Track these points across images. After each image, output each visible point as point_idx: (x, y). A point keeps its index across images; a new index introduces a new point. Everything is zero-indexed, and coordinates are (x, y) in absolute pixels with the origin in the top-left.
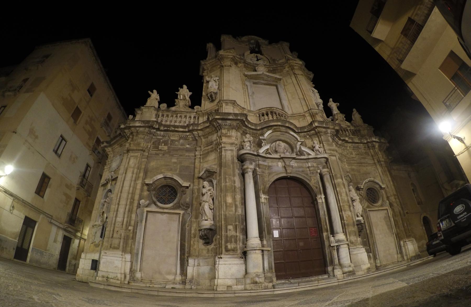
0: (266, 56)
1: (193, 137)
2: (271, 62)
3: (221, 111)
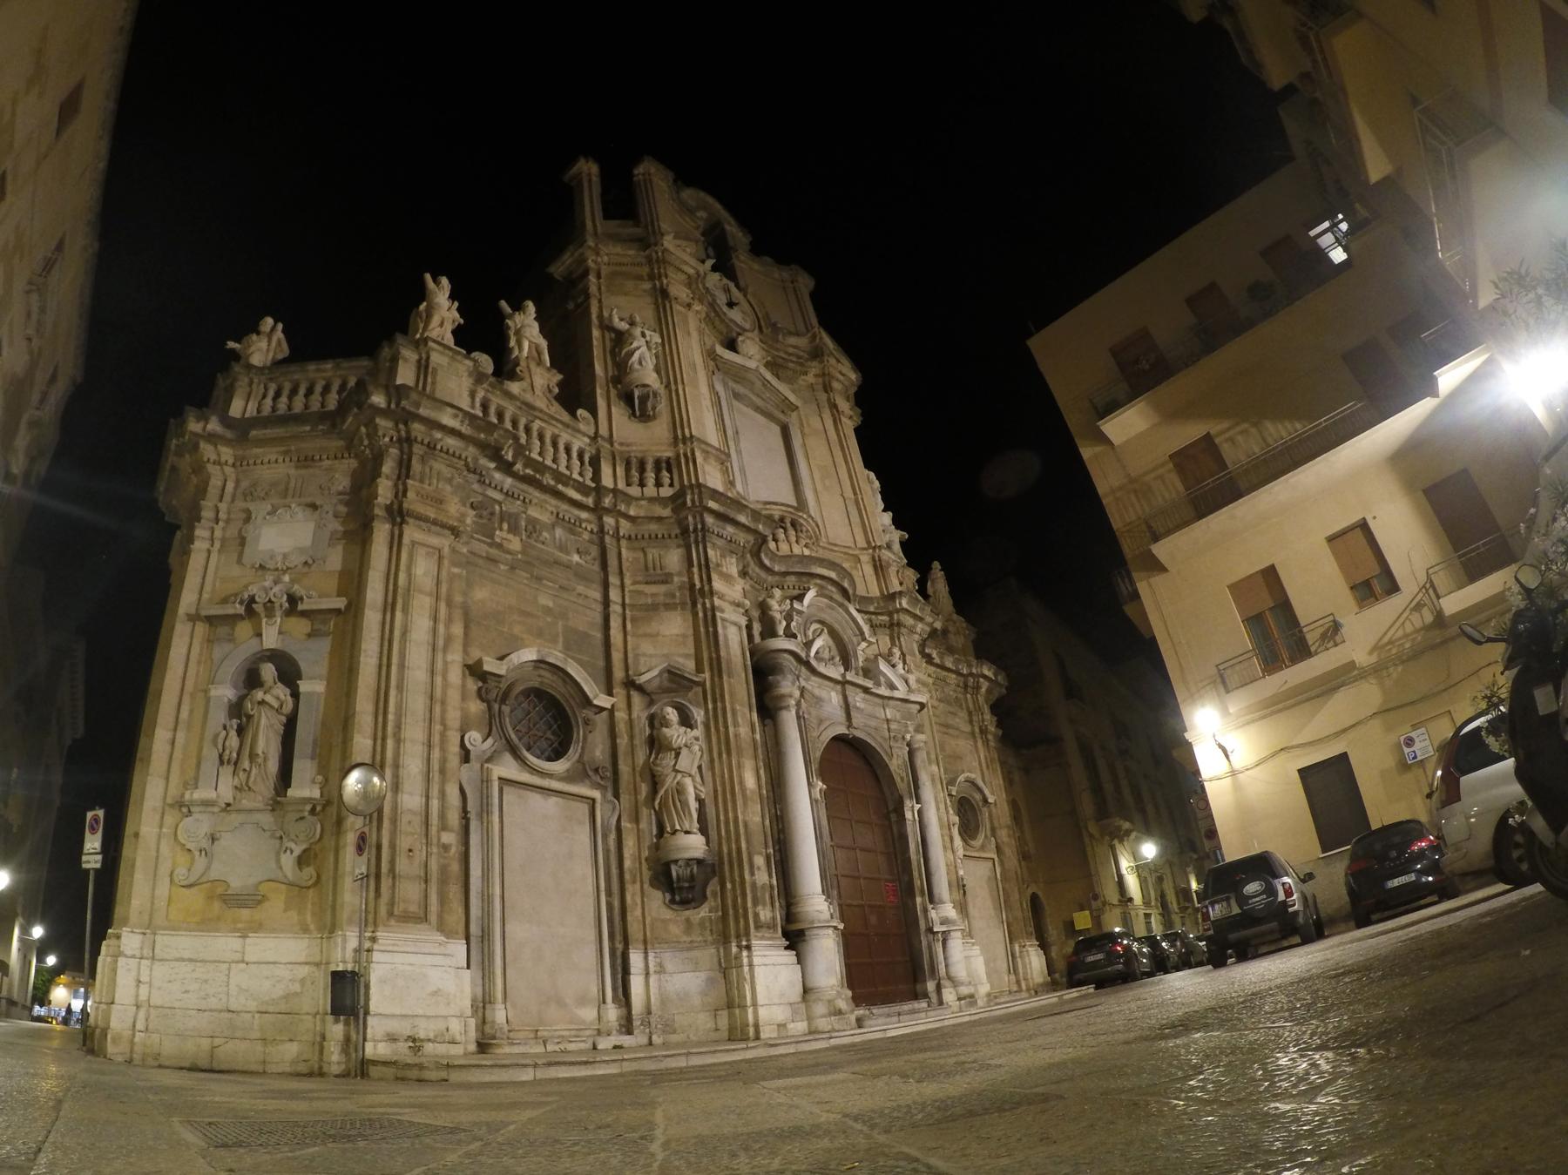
0: (751, 300)
1: (595, 530)
2: (764, 330)
3: (690, 479)
